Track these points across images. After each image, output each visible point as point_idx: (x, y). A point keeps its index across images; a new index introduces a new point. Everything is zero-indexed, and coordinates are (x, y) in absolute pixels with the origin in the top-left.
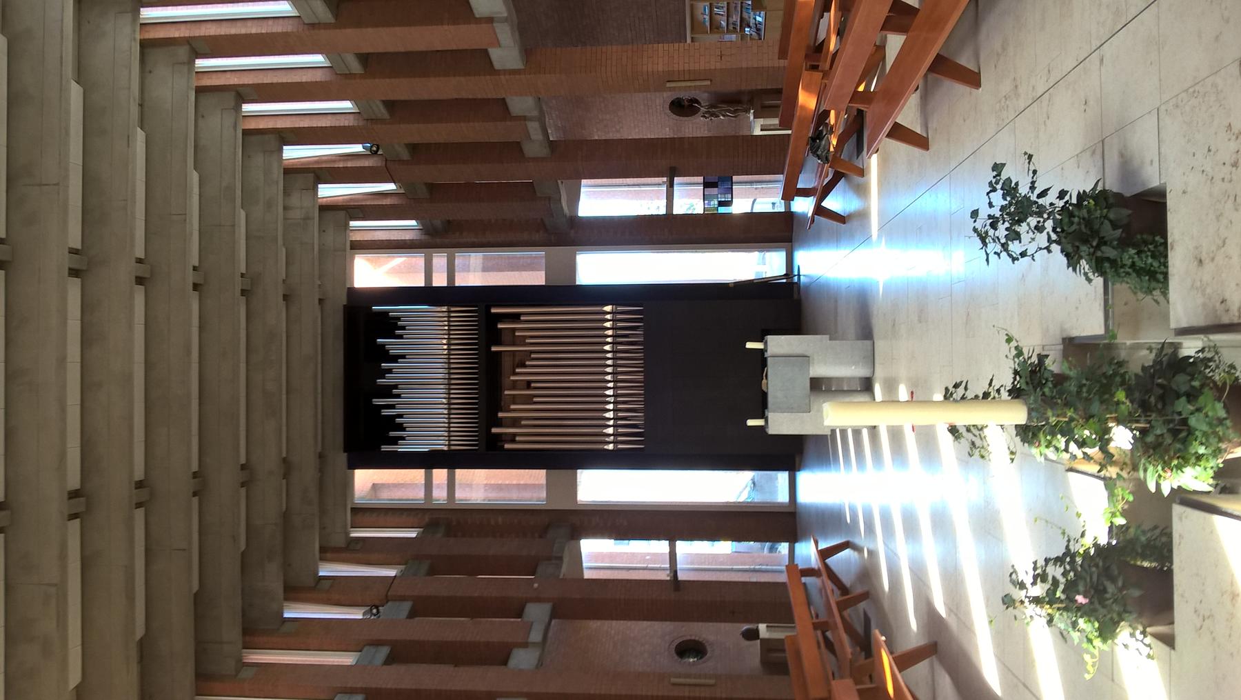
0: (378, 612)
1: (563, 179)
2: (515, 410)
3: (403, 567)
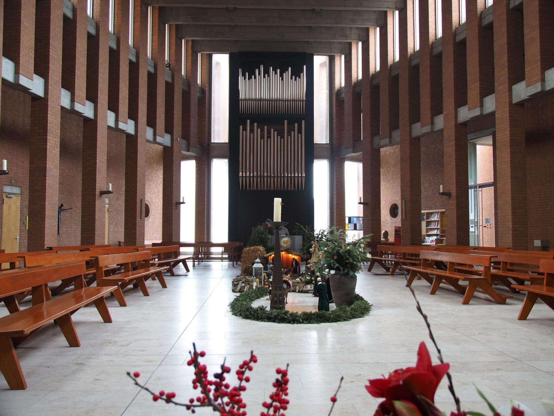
0: (167, 67)
1: (363, 154)
2: (257, 130)
3: (185, 78)
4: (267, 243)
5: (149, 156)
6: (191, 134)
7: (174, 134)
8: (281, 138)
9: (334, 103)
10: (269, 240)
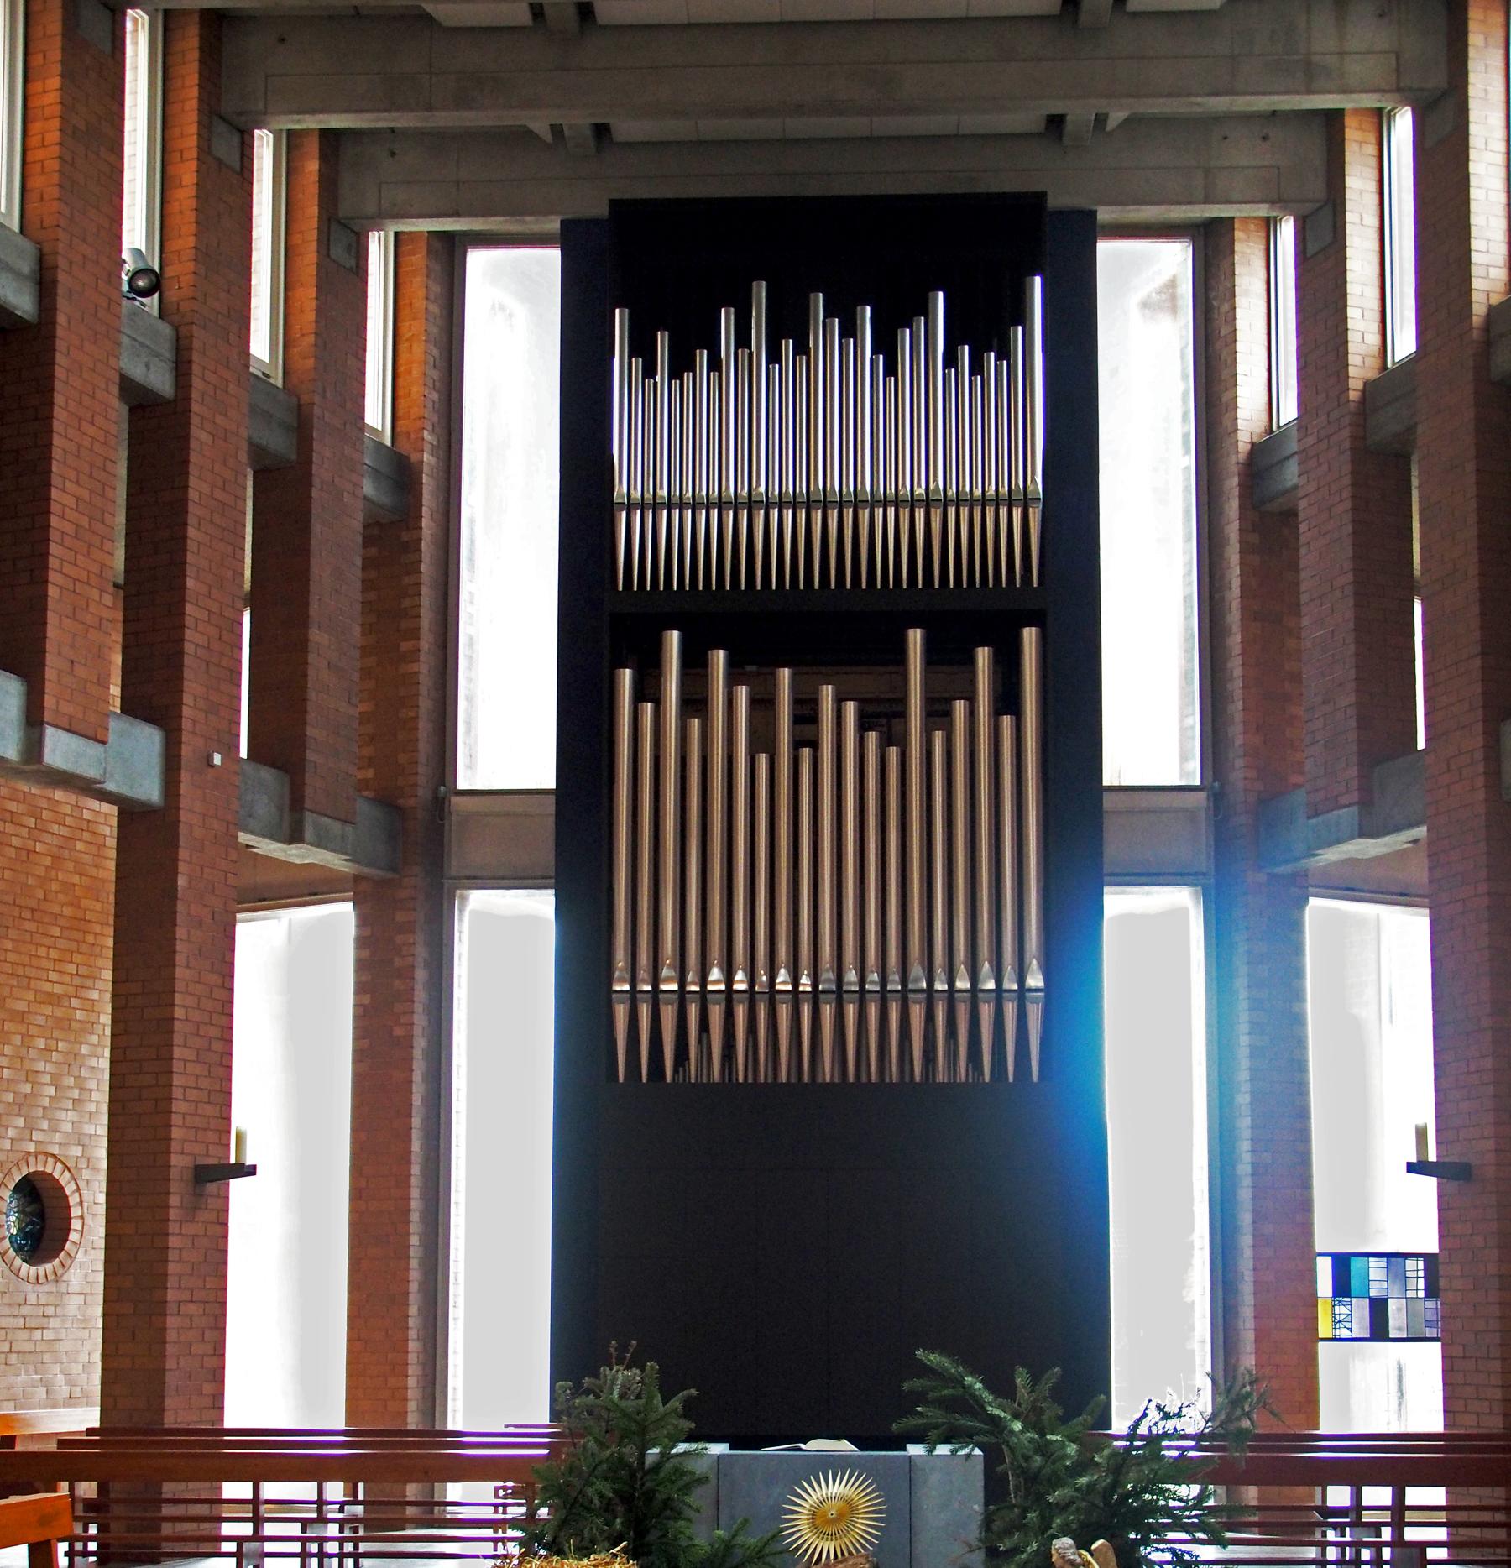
4: (678, 1516)
5: (76, 879)
6: (310, 731)
7: (186, 724)
8: (885, 742)
9: (1232, 530)
10: (698, 1491)
